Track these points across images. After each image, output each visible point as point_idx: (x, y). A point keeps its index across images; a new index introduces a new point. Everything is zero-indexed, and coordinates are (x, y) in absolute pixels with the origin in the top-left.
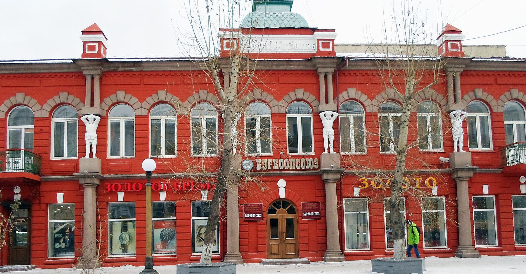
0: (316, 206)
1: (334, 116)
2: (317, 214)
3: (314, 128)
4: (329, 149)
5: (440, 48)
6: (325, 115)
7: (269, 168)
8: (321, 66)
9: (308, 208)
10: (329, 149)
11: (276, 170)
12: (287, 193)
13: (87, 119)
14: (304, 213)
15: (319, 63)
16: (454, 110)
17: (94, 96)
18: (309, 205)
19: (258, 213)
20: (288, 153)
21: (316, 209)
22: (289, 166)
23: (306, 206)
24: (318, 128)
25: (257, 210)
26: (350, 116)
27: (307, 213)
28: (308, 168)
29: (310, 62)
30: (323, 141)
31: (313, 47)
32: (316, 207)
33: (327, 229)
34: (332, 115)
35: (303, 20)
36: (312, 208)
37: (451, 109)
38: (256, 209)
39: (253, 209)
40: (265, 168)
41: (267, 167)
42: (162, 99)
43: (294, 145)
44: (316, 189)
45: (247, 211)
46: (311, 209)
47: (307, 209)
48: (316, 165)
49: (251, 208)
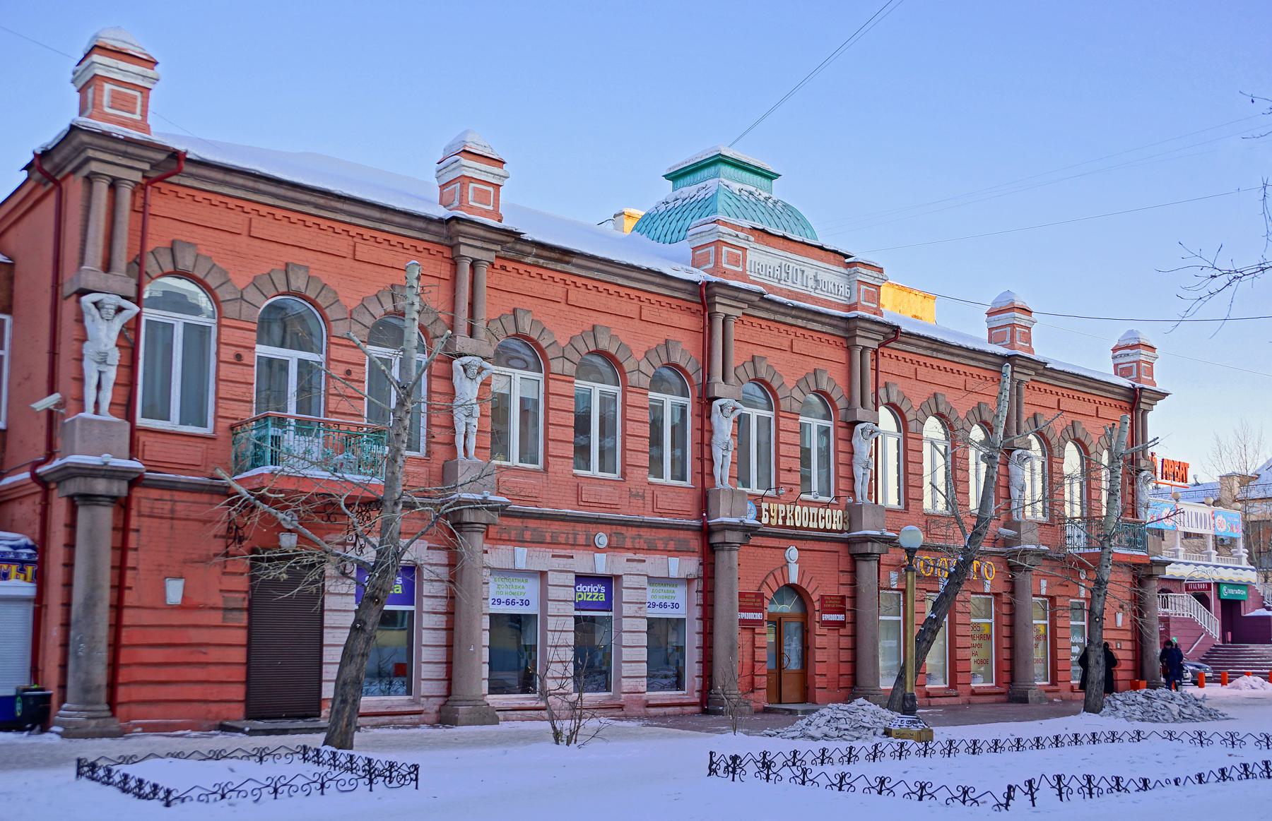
1: (125, 311)
2: (841, 617)
4: (97, 404)
5: (698, 252)
6: (95, 304)
7: (780, 522)
8: (862, 334)
10: (97, 404)
11: (790, 527)
12: (802, 574)
13: (95, 304)
15: (466, 235)
16: (466, 355)
26: (512, 375)
34: (120, 310)
35: (806, 226)
37: (859, 418)
40: (774, 522)
42: (299, 287)
43: (582, 452)
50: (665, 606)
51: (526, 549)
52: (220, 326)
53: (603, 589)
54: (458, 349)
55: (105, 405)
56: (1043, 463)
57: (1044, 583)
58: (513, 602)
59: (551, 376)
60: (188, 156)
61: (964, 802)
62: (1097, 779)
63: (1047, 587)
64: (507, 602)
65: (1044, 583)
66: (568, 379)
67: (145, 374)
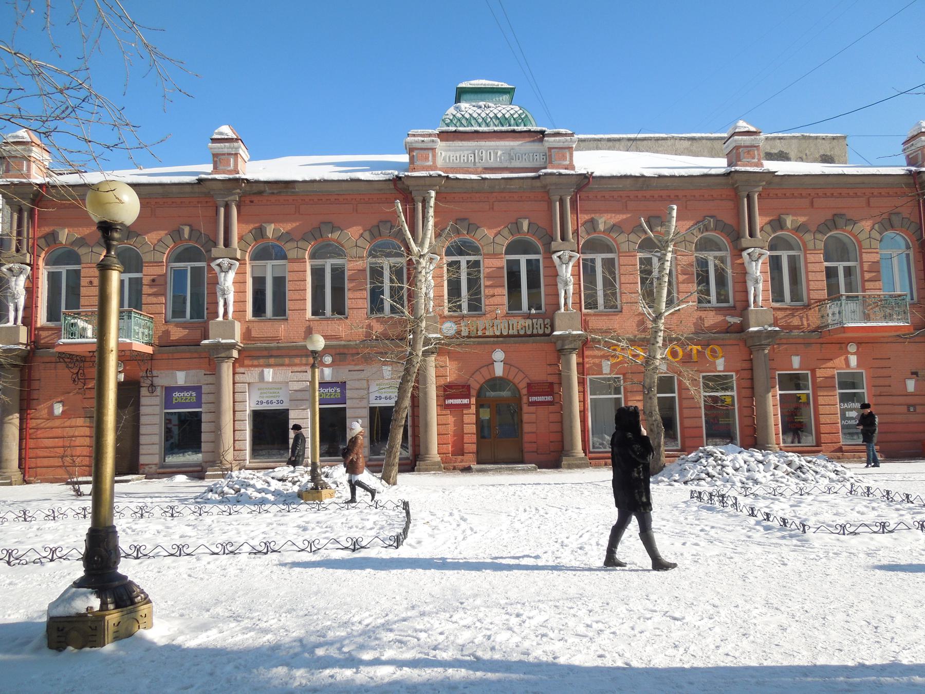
28: (535, 332)
29: (538, 180)
30: (557, 295)
34: (761, 255)
50: (272, 402)
51: (271, 370)
52: (619, 256)
53: (338, 390)
54: (744, 245)
55: (570, 305)
56: (908, 255)
57: (499, 355)
58: (272, 402)
59: (863, 250)
60: (594, 175)
61: (9, 563)
62: (893, 494)
63: (492, 362)
64: (386, 398)
65: (499, 355)
66: (875, 251)
67: (60, 294)
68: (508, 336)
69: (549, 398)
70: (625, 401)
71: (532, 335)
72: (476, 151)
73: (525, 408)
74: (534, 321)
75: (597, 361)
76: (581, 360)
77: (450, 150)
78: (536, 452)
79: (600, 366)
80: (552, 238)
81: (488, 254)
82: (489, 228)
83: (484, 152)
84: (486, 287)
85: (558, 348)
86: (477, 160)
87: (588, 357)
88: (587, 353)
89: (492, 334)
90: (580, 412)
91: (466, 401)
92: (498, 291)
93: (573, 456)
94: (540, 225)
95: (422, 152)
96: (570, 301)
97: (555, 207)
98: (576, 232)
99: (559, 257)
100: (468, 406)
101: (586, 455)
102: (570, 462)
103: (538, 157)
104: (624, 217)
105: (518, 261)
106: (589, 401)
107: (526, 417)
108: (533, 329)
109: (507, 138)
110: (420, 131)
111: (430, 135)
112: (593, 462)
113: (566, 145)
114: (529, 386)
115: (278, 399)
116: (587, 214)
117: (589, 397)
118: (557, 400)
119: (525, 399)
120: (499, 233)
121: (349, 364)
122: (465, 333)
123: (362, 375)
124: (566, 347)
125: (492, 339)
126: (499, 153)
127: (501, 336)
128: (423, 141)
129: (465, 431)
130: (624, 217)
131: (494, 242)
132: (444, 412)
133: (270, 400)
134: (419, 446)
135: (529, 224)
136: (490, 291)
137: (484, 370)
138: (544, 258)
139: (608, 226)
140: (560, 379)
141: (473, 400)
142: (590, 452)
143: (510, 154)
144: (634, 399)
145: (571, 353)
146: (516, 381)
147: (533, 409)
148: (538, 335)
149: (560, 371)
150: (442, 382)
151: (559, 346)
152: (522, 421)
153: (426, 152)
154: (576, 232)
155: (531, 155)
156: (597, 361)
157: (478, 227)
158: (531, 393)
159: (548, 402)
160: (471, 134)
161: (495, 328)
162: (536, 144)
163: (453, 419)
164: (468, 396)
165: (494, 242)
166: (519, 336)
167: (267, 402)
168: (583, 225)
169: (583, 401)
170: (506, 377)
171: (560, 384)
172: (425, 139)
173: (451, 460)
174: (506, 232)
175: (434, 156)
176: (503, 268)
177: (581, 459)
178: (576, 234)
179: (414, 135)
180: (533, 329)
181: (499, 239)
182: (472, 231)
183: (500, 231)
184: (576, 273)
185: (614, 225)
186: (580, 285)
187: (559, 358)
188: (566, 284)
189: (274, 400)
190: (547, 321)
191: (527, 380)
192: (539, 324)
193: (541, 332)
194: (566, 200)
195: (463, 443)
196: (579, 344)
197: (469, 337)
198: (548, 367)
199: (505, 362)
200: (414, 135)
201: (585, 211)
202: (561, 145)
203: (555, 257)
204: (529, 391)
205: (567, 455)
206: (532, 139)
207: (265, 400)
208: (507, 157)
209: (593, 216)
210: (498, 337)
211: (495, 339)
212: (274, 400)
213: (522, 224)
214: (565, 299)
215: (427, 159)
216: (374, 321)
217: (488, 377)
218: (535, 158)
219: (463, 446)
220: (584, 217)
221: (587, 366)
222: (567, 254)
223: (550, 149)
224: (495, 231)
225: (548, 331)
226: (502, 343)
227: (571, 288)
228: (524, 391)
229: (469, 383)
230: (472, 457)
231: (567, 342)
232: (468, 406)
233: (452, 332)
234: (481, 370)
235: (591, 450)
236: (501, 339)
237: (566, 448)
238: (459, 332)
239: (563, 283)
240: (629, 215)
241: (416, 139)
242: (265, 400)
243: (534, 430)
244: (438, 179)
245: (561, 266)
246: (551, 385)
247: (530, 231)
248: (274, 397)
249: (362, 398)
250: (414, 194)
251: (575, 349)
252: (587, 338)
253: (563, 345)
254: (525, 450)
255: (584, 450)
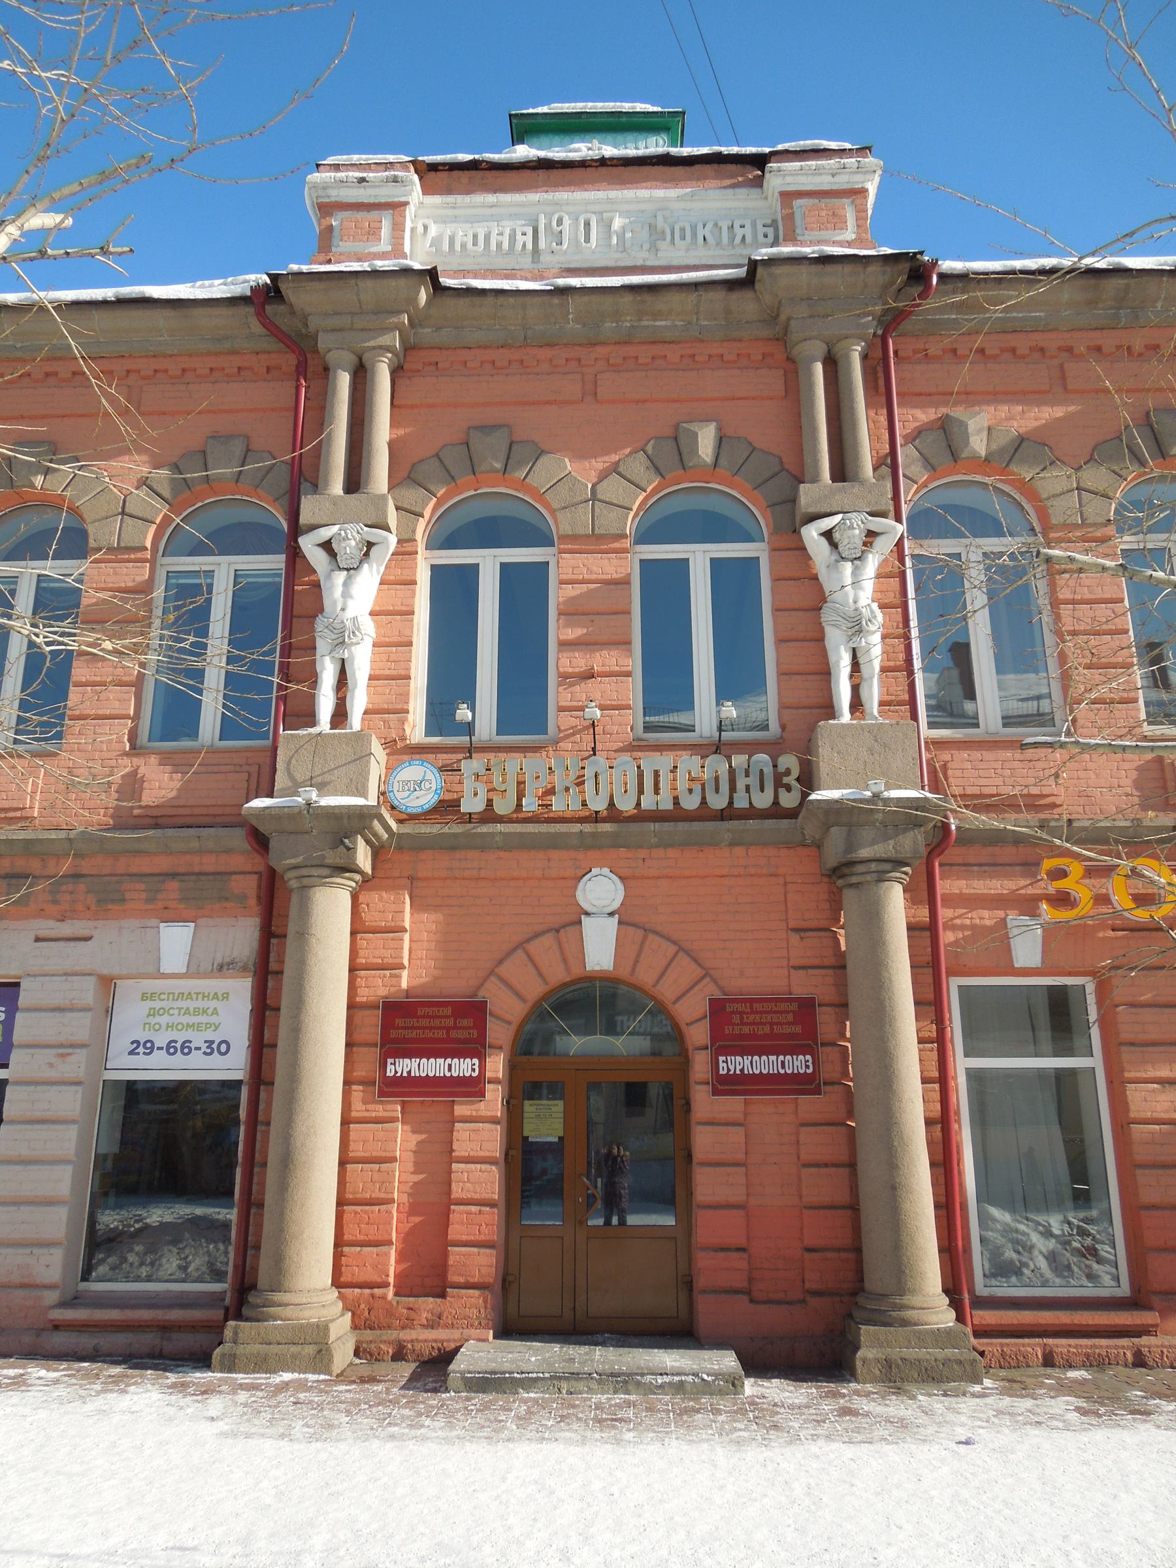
0: (790, 1018)
3: (776, 610)
9: (746, 1030)
14: (721, 1059)
17: (1065, 1157)
18: (752, 1012)
19: (794, 1051)
20: (849, 1045)
21: (792, 1036)
22: (641, 791)
23: (736, 1019)
24: (791, 579)
25: (454, 1034)
27: (739, 1059)
28: (741, 803)
29: (747, 294)
30: (825, 673)
31: (766, 236)
32: (789, 1023)
33: (866, 1241)
36: (767, 1029)
38: (448, 1029)
39: (431, 1028)
41: (520, 795)
44: (792, 924)
45: (396, 1041)
46: (765, 1037)
47: (741, 1037)
48: (789, 788)
49: (425, 1022)
50: (186, 1048)
63: (575, 918)
64: (170, 1048)
68: (642, 816)
69: (798, 1064)
70: (1110, 1082)
71: (728, 814)
72: (542, 222)
73: (703, 1102)
74: (739, 760)
75: (987, 917)
76: (923, 914)
77: (455, 219)
78: (749, 1292)
79: (1001, 938)
80: (800, 475)
81: (574, 538)
82: (580, 455)
83: (567, 221)
84: (564, 645)
85: (832, 862)
86: (542, 244)
87: (949, 901)
88: (944, 886)
89: (575, 806)
90: (929, 1122)
91: (464, 1067)
92: (603, 660)
93: (905, 1323)
94: (756, 444)
95: (360, 215)
96: (873, 693)
97: (810, 374)
98: (889, 463)
99: (828, 535)
100: (472, 1087)
101: (960, 1318)
102: (896, 1353)
103: (748, 231)
104: (1059, 412)
105: (682, 565)
106: (962, 1080)
107: (703, 1141)
108: (733, 789)
109: (645, 179)
110: (355, 158)
111: (389, 166)
112: (993, 1345)
113: (843, 181)
114: (718, 1010)
115: (209, 1035)
116: (921, 406)
117: (961, 1064)
118: (829, 1071)
119: (700, 1065)
120: (615, 469)
121: (41, 914)
122: (472, 804)
123: (79, 956)
124: (864, 853)
125: (576, 828)
126: (617, 223)
127: (613, 814)
128: (362, 180)
129: (457, 1192)
130: (1059, 412)
131: (594, 497)
132: (378, 1110)
133: (181, 1037)
134: (257, 1247)
135: (720, 440)
136: (578, 661)
137: (543, 948)
138: (774, 550)
139: (1002, 440)
140: (842, 985)
141: (497, 1065)
142: (982, 1303)
143: (652, 227)
144: (1152, 1073)
145: (881, 878)
146: (667, 991)
147: (732, 1105)
148: (752, 813)
149: (842, 955)
150: (376, 988)
151: (834, 851)
152: (689, 1156)
153: (374, 214)
154: (889, 463)
155: (725, 225)
156: (987, 917)
157: (543, 452)
158: (722, 1044)
159: (795, 1078)
160: (527, 173)
161: (589, 786)
162: (742, 192)
163: (415, 1139)
164: (476, 1048)
165: (594, 497)
166: (677, 814)
167: (170, 1048)
168: (910, 439)
169: (939, 1079)
170: (624, 973)
171: (842, 1006)
172: (370, 175)
173: (390, 1312)
174: (638, 467)
175: (398, 228)
176: (626, 582)
177: (943, 1338)
178: (885, 470)
179: (336, 167)
180: (733, 789)
181: (613, 489)
182: (520, 464)
183: (617, 463)
184: (893, 597)
185: (1022, 440)
186: (907, 637)
187: (836, 906)
188: (857, 627)
189: (198, 1040)
190: (789, 761)
191: (710, 990)
192: (755, 773)
193: (763, 800)
194: (847, 358)
195: (445, 1244)
196: (912, 842)
197: (489, 815)
198: (794, 938)
199: (625, 918)
200: (336, 167)
201: (914, 397)
202: (824, 182)
203: (812, 534)
204: (716, 1033)
205: (881, 1319)
206: (728, 182)
207: (161, 1040)
208: (644, 234)
209: (943, 410)
210: (596, 818)
211: (588, 828)
212: (198, 1040)
213: (694, 436)
214: (855, 689)
215: (373, 233)
216: (153, 759)
217: (558, 975)
218: (739, 233)
219: (446, 1255)
220: (909, 418)
221: (947, 937)
222: (858, 524)
223: (788, 197)
224: (600, 464)
225: (789, 800)
226: (615, 842)
227: (875, 650)
228: (699, 1034)
229: (482, 994)
230: (471, 1303)
231: (867, 833)
232: (472, 1087)
233: (425, 800)
234: (533, 947)
235: (981, 1289)
236: (607, 827)
237: (875, 1279)
238: (447, 808)
239: (844, 625)
240: (1072, 408)
241: (341, 175)
242: (161, 1040)
243: (736, 1194)
244: (402, 282)
245: (833, 567)
246: (807, 1007)
247: (723, 461)
248: (197, 1027)
249: (67, 1047)
250: (323, 342)
251: (899, 863)
252: (946, 827)
253: (850, 846)
254: (701, 1282)
255: (952, 1290)
